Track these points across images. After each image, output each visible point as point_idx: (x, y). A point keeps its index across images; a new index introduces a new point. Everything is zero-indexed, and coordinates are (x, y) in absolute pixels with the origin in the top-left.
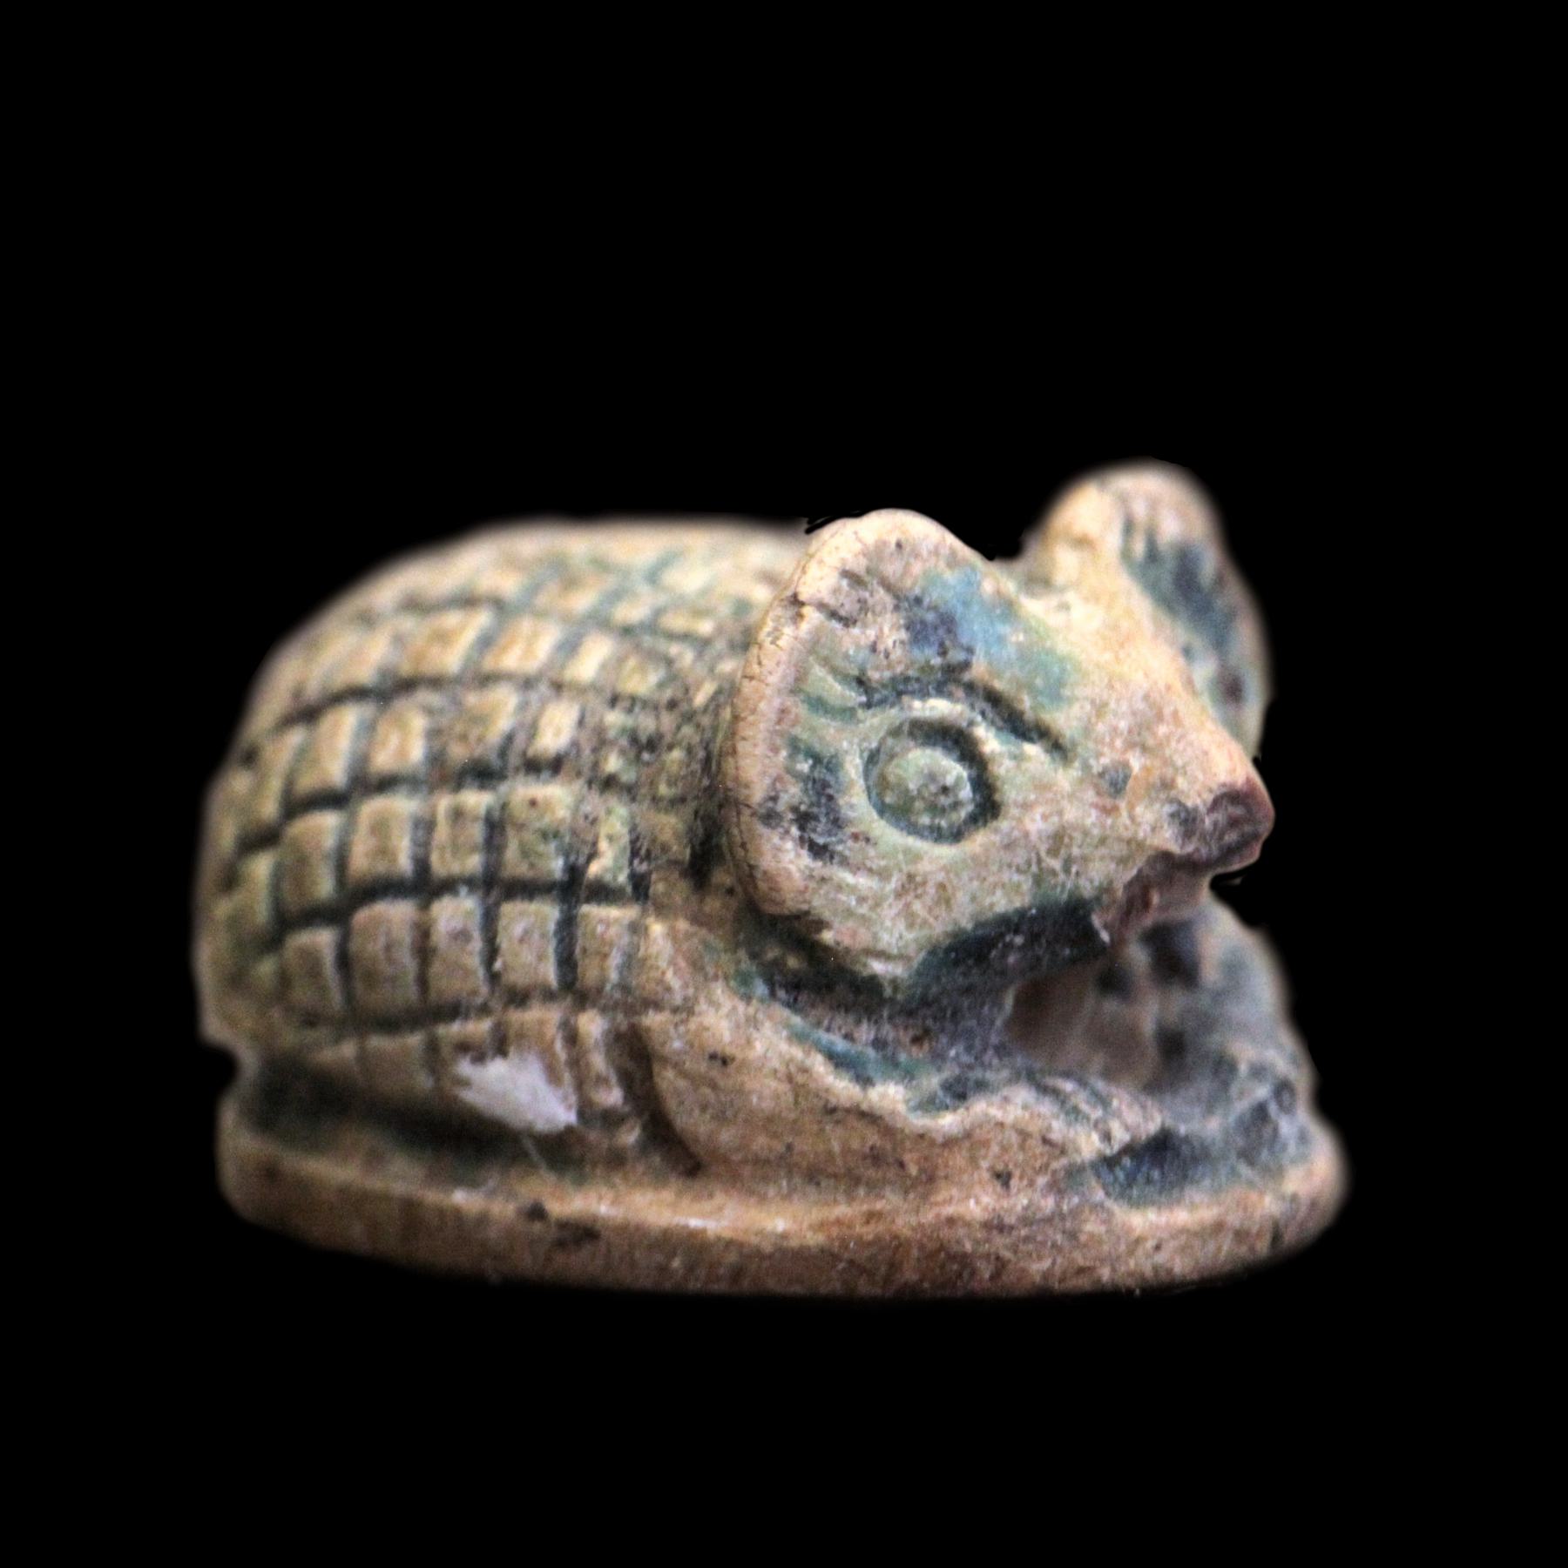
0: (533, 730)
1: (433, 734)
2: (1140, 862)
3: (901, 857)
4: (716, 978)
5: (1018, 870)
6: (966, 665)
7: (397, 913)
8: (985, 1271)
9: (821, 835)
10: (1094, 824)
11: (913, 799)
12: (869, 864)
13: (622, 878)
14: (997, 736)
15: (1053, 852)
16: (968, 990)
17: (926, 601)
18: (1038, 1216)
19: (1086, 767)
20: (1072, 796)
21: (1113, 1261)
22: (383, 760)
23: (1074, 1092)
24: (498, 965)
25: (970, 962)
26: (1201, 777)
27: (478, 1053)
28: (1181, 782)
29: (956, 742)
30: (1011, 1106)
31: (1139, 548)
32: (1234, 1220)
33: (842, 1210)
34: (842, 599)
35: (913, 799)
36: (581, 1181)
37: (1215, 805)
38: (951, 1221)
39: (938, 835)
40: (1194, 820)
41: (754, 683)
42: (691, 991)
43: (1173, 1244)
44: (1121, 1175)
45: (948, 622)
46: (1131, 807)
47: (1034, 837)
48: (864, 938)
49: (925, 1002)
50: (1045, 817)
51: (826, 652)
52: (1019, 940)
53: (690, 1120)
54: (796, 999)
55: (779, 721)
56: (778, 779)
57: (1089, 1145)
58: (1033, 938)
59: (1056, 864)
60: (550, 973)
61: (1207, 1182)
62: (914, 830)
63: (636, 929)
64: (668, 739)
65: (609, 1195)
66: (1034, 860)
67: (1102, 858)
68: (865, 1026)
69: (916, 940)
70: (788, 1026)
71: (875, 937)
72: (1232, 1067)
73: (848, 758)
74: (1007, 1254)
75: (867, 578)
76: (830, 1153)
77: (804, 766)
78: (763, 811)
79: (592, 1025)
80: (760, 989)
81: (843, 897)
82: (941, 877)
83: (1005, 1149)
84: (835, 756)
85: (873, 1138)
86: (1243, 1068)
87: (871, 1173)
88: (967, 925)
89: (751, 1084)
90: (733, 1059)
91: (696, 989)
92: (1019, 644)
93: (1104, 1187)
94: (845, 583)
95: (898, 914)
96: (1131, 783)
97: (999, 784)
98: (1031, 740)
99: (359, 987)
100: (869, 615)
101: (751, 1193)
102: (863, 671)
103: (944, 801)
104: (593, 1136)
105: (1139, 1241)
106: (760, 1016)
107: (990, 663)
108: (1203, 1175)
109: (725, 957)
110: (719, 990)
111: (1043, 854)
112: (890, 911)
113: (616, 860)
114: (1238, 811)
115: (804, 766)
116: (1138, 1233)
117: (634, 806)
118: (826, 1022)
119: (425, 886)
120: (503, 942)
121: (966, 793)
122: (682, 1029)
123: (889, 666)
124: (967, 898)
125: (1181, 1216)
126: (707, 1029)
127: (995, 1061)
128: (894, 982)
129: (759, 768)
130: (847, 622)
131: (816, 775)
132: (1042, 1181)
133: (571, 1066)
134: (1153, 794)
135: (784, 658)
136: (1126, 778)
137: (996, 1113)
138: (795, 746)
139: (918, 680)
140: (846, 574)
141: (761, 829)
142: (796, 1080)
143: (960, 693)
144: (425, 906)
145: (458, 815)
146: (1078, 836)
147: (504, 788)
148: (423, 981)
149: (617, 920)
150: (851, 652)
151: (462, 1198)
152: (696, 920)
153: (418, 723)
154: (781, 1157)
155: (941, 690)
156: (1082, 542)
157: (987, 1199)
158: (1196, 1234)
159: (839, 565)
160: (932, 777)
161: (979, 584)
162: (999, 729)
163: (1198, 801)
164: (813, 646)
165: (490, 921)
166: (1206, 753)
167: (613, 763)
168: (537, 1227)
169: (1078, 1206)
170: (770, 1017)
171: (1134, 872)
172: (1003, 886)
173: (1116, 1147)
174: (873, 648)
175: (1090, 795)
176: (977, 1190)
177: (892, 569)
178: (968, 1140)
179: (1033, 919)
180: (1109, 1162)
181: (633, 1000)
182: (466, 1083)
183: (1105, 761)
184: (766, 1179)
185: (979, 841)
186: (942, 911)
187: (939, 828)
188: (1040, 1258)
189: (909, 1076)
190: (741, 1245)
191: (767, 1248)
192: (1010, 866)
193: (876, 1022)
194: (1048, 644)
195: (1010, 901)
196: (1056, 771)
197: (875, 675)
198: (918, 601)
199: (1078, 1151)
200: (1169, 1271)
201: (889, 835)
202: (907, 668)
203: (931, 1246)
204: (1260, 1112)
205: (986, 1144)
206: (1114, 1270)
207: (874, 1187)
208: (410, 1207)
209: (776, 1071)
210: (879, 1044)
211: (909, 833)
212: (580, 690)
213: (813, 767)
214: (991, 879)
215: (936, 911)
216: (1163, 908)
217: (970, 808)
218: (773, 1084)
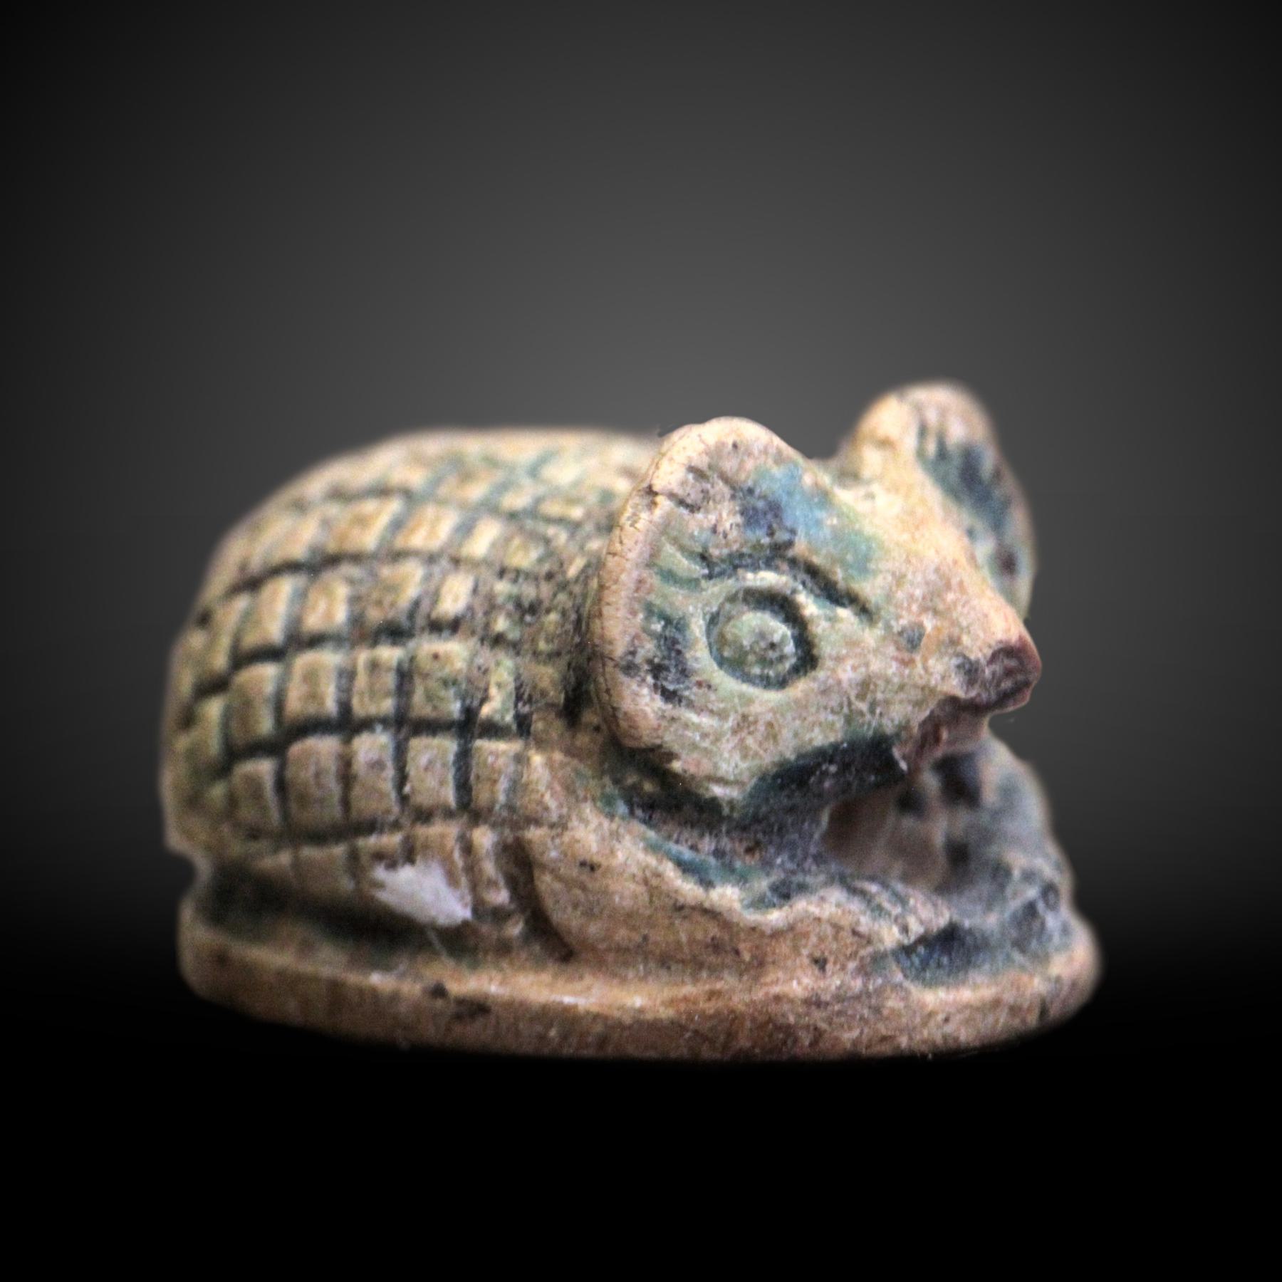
0: (436, 597)
1: (354, 600)
2: (932, 705)
3: (736, 700)
4: (585, 799)
5: (833, 712)
6: (790, 544)
7: (325, 747)
8: (806, 1039)
9: (671, 682)
10: (894, 674)
11: (746, 653)
12: (710, 706)
13: (509, 718)
14: (815, 602)
15: (861, 697)
16: (792, 810)
17: (757, 491)
18: (849, 994)
19: (888, 627)
20: (876, 651)
21: (910, 1031)
22: (314, 621)
23: (878, 893)
24: (407, 789)
25: (793, 787)
26: (982, 635)
27: (391, 861)
28: (966, 640)
29: (782, 607)
30: (826, 905)
31: (931, 448)
32: (1009, 997)
33: (688, 989)
34: (688, 489)
35: (746, 653)
36: (475, 966)
37: (994, 658)
38: (778, 998)
39: (767, 683)
40: (976, 670)
41: (616, 558)
42: (565, 810)
43: (959, 1017)
44: (916, 961)
45: (775, 509)
46: (925, 660)
47: (845, 684)
48: (706, 767)
49: (756, 819)
50: (854, 668)
51: (675, 533)
52: (833, 769)
53: (564, 916)
54: (650, 817)
55: (637, 590)
56: (636, 637)
57: (890, 936)
58: (845, 767)
59: (863, 706)
60: (449, 795)
61: (987, 967)
62: (747, 678)
63: (520, 759)
64: (546, 604)
65: (498, 977)
66: (846, 703)
67: (901, 702)
68: (707, 839)
69: (749, 769)
70: (644, 839)
71: (716, 766)
72: (1007, 873)
73: (694, 620)
74: (823, 1026)
75: (709, 473)
76: (678, 943)
77: (658, 627)
78: (624, 663)
79: (484, 838)
80: (622, 808)
81: (689, 734)
82: (769, 717)
83: (821, 939)
84: (683, 618)
85: (714, 931)
86: (1016, 873)
87: (712, 959)
88: (791, 756)
89: (614, 886)
90: (599, 866)
91: (569, 808)
92: (833, 527)
93: (903, 970)
94: (691, 476)
95: (734, 748)
96: (924, 640)
97: (816, 641)
98: (843, 605)
99: (294, 807)
100: (711, 503)
101: (614, 975)
102: (705, 549)
103: (772, 655)
104: (485, 929)
105: (931, 1015)
106: (622, 831)
107: (809, 542)
108: (984, 961)
109: (593, 783)
110: (588, 809)
111: (853, 698)
112: (728, 745)
113: (503, 703)
114: (1012, 663)
115: (658, 627)
116: (930, 1008)
117: (519, 659)
118: (675, 836)
119: (347, 724)
120: (412, 770)
121: (790, 648)
122: (557, 841)
123: (727, 545)
124: (791, 735)
125: (966, 995)
126: (578, 841)
127: (814, 868)
128: (731, 803)
129: (620, 628)
130: (693, 508)
131: (667, 633)
132: (852, 965)
133: (467, 871)
134: (943, 650)
135: (641, 538)
136: (921, 636)
137: (814, 910)
138: (650, 610)
139: (750, 556)
140: (692, 469)
141: (622, 678)
142: (651, 883)
143: (785, 567)
144: (347, 741)
145: (374, 666)
146: (881, 683)
147: (412, 644)
148: (346, 802)
149: (504, 753)
150: (696, 533)
151: (377, 980)
152: (569, 752)
153: (342, 591)
154: (639, 946)
155: (769, 564)
156: (885, 443)
157: (807, 981)
158: (978, 1009)
159: (686, 462)
160: (762, 635)
161: (801, 478)
162: (817, 596)
163: (980, 655)
164: (665, 528)
165: (400, 753)
166: (986, 616)
167: (501, 624)
168: (439, 1003)
169: (881, 986)
170: (630, 832)
171: (927, 713)
172: (820, 724)
173: (913, 938)
174: (714, 530)
175: (891, 650)
176: (799, 973)
177: (729, 465)
178: (791, 932)
179: (845, 751)
180: (906, 950)
181: (517, 818)
182: (381, 885)
183: (903, 622)
184: (626, 964)
185: (801, 688)
186: (770, 745)
187: (768, 677)
188: (850, 1029)
189: (743, 879)
190: (606, 1018)
191: (627, 1020)
192: (825, 708)
193: (716, 836)
194: (857, 526)
195: (826, 737)
196: (863, 630)
197: (715, 552)
198: (751, 491)
199: (881, 941)
200: (956, 1039)
201: (727, 683)
202: (742, 546)
203: (761, 1019)
204: (1030, 909)
205: (806, 935)
206: (911, 1038)
207: (715, 971)
208: (335, 987)
209: (634, 876)
210: (718, 853)
211: (744, 681)
212: (474, 564)
213: (665, 627)
214: (810, 719)
215: (766, 745)
216: (951, 742)
217: (793, 660)
218: (632, 886)
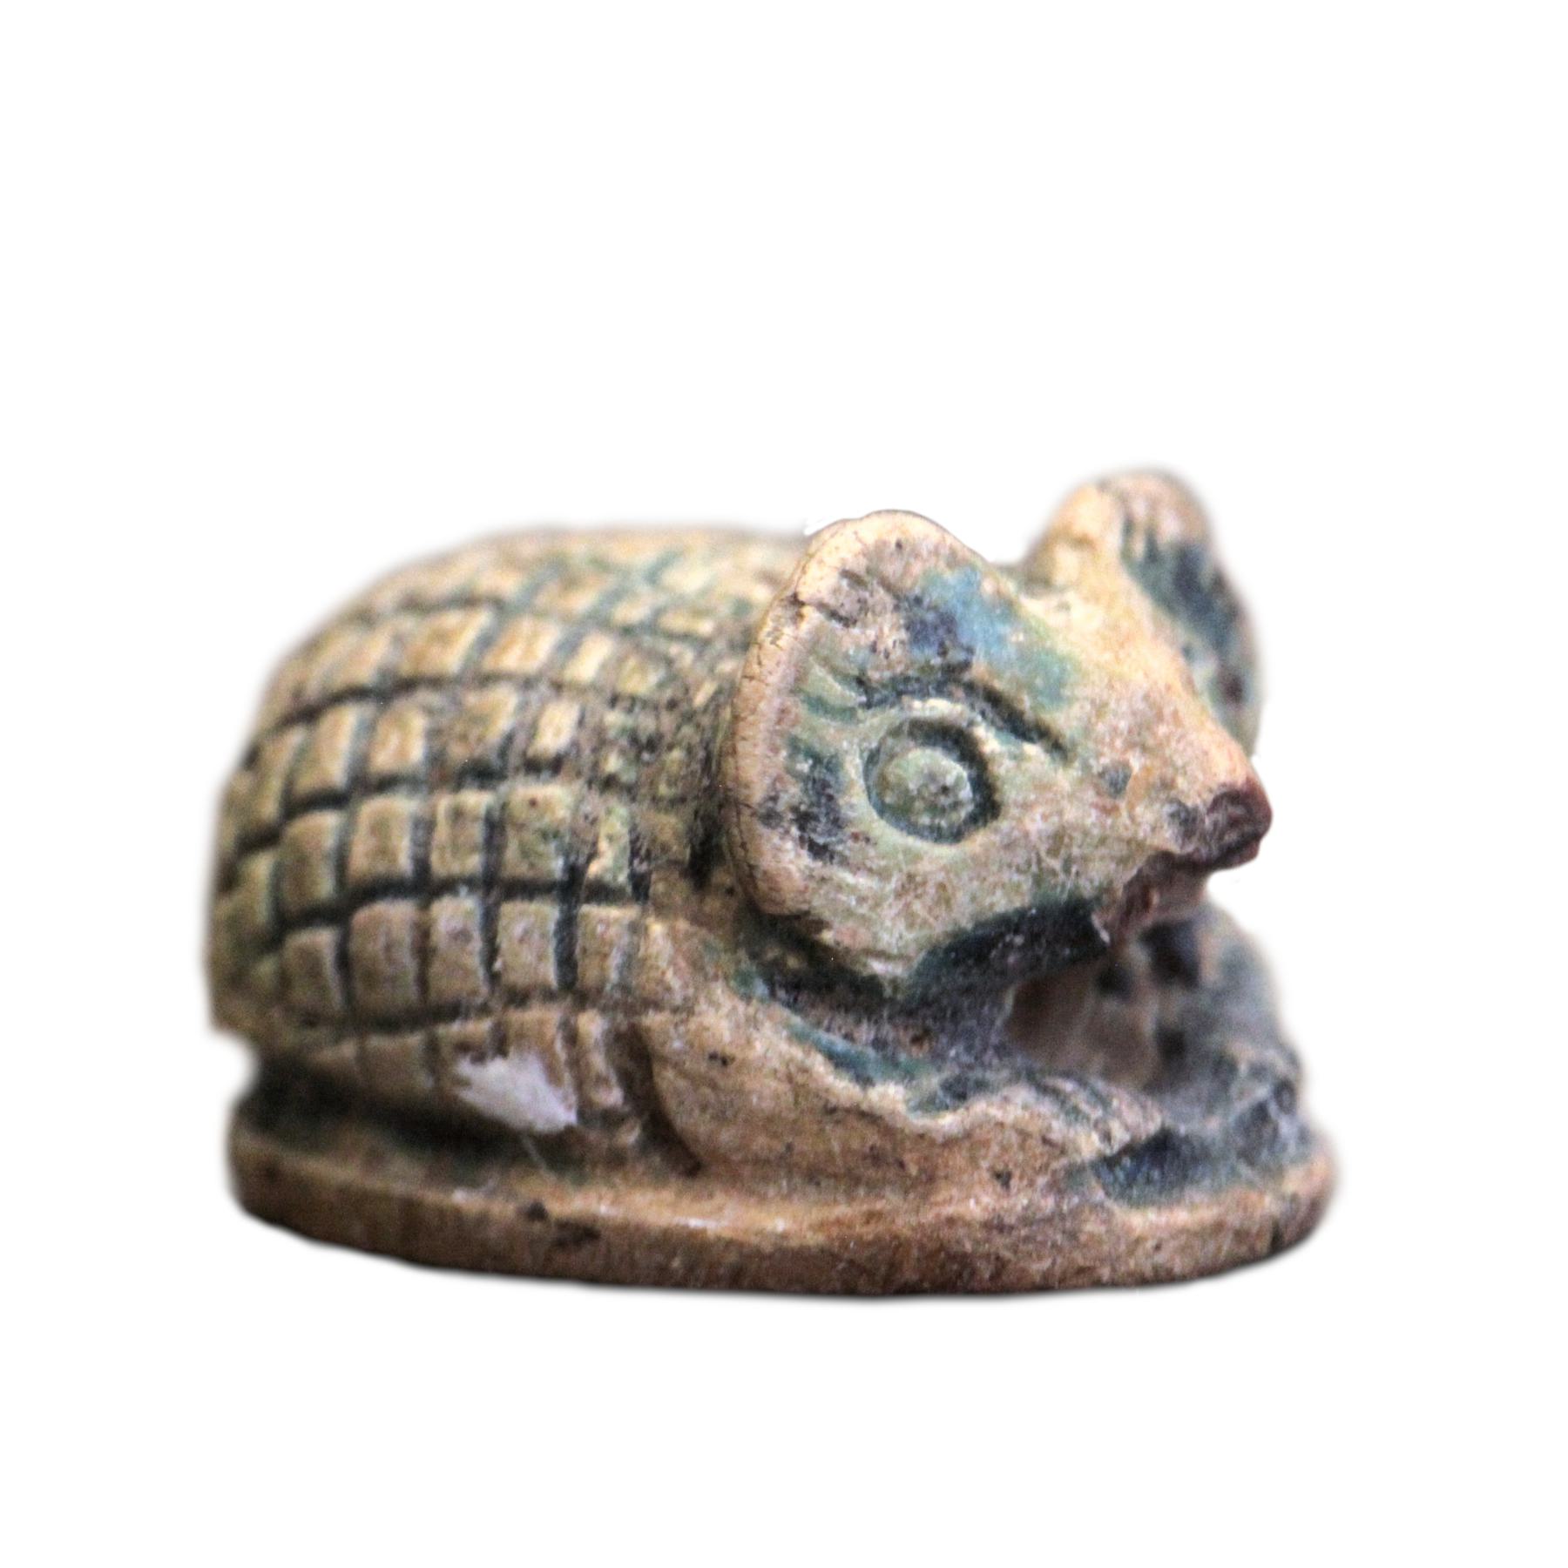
0: (533, 730)
1: (433, 734)
2: (1140, 862)
3: (901, 857)
4: (716, 978)
5: (1018, 870)
6: (966, 665)
7: (397, 913)
9: (821, 835)
10: (1094, 824)
11: (913, 799)
12: (869, 864)
13: (622, 878)
14: (997, 736)
15: (1053, 852)
16: (968, 990)
17: (926, 601)
18: (1038, 1216)
19: (1086, 767)
20: (1072, 796)
22: (383, 760)
23: (1074, 1092)
24: (498, 965)
25: (970, 962)
26: (1201, 777)
27: (478, 1053)
28: (1181, 782)
29: (956, 742)
30: (1011, 1106)
31: (1139, 548)
32: (1234, 1220)
33: (842, 1210)
34: (842, 599)
35: (913, 799)
36: (581, 1181)
37: (1215, 805)
38: (951, 1221)
39: (938, 835)
40: (1194, 820)
41: (754, 683)
42: (691, 991)
43: (1173, 1244)
44: (1121, 1175)
45: (948, 622)
46: (1131, 807)
47: (1034, 837)
48: (864, 938)
49: (925, 1002)
50: (1045, 817)
51: (826, 652)
52: (1019, 940)
53: (690, 1120)
54: (796, 999)
55: (779, 721)
56: (778, 779)
57: (1089, 1145)
58: (1033, 938)
59: (1056, 864)
60: (550, 973)
61: (1207, 1182)
62: (914, 830)
63: (636, 929)
64: (668, 739)
65: (609, 1195)
66: (1034, 860)
67: (1102, 858)
68: (865, 1026)
69: (916, 940)
70: (788, 1026)
71: (875, 937)
72: (1232, 1067)
73: (848, 758)
74: (1007, 1254)
75: (867, 578)
76: (830, 1153)
77: (804, 766)
78: (763, 811)
79: (592, 1025)
80: (760, 989)
81: (843, 897)
82: (941, 877)
83: (1005, 1149)
84: (835, 756)
85: (873, 1138)
86: (1243, 1068)
87: (871, 1173)
88: (967, 925)
89: (751, 1084)
90: (733, 1059)
91: (696, 989)
92: (1019, 644)
93: (1104, 1187)
94: (845, 583)
95: (898, 914)
96: (1131, 783)
97: (999, 784)
98: (1031, 740)
99: (359, 987)
100: (869, 615)
101: (751, 1193)
102: (863, 671)
103: (944, 801)
104: (593, 1136)
105: (1139, 1241)
106: (760, 1016)
107: (990, 663)
108: (1203, 1175)
109: (725, 957)
110: (719, 990)
111: (1043, 854)
112: (890, 911)
113: (616, 860)
114: (1238, 811)
115: (804, 766)
116: (1138, 1233)
117: (634, 806)
118: (826, 1022)
119: (425, 886)
120: (503, 942)
121: (966, 793)
122: (682, 1029)
123: (889, 666)
124: (967, 898)
125: (1181, 1216)
126: (707, 1029)
127: (995, 1061)
128: (894, 982)
129: (759, 768)
130: (847, 622)
131: (816, 775)
132: (1042, 1181)
133: (571, 1066)
134: (1153, 794)
135: (784, 658)
136: (1126, 778)
137: (996, 1113)
138: (795, 746)
139: (918, 680)
140: (846, 574)
141: (761, 829)
142: (796, 1080)
143: (960, 693)
144: (425, 906)
145: (458, 815)
146: (1078, 836)
147: (504, 788)
148: (423, 981)
149: (617, 920)
150: (851, 652)
151: (462, 1198)
152: (696, 920)
153: (418, 723)
154: (781, 1157)
155: (941, 690)
157: (987, 1199)
158: (1196, 1234)
159: (839, 565)
160: (932, 777)
161: (979, 584)
162: (999, 729)
163: (1198, 801)
164: (813, 646)
165: (490, 921)
166: (1206, 753)
167: (613, 763)
168: (537, 1227)
169: (1078, 1206)
170: (770, 1017)
171: (1134, 872)
172: (1003, 886)
173: (1116, 1147)
174: (873, 648)
175: (1090, 795)
176: (977, 1190)
177: (892, 569)
178: (968, 1140)
179: (1033, 919)
180: (1109, 1162)
181: (633, 1000)
182: (466, 1083)
183: (1105, 761)
184: (766, 1179)
185: (979, 841)
186: (942, 911)
187: (939, 828)
188: (1040, 1258)
189: (909, 1076)
190: (741, 1245)
191: (767, 1248)
192: (1010, 866)
193: (876, 1022)
194: (1048, 644)
195: (1010, 901)
196: (1056, 771)
197: (875, 675)
198: (918, 601)
199: (1078, 1151)
201: (889, 835)
202: (907, 668)
203: (931, 1246)
204: (1260, 1112)
205: (986, 1144)
207: (874, 1187)
209: (776, 1071)
210: (879, 1044)
211: (909, 833)
212: (580, 690)
213: (813, 767)
214: (991, 879)
215: (936, 911)
216: (1163, 908)
217: (970, 808)
218: (773, 1084)
